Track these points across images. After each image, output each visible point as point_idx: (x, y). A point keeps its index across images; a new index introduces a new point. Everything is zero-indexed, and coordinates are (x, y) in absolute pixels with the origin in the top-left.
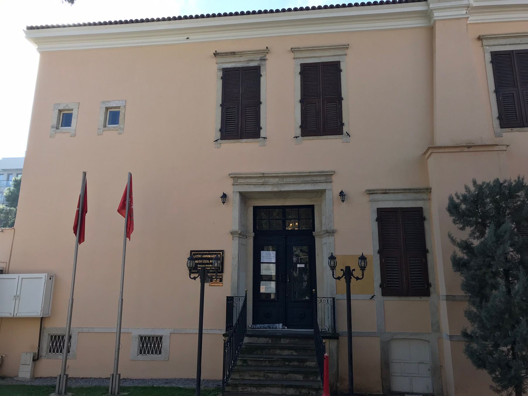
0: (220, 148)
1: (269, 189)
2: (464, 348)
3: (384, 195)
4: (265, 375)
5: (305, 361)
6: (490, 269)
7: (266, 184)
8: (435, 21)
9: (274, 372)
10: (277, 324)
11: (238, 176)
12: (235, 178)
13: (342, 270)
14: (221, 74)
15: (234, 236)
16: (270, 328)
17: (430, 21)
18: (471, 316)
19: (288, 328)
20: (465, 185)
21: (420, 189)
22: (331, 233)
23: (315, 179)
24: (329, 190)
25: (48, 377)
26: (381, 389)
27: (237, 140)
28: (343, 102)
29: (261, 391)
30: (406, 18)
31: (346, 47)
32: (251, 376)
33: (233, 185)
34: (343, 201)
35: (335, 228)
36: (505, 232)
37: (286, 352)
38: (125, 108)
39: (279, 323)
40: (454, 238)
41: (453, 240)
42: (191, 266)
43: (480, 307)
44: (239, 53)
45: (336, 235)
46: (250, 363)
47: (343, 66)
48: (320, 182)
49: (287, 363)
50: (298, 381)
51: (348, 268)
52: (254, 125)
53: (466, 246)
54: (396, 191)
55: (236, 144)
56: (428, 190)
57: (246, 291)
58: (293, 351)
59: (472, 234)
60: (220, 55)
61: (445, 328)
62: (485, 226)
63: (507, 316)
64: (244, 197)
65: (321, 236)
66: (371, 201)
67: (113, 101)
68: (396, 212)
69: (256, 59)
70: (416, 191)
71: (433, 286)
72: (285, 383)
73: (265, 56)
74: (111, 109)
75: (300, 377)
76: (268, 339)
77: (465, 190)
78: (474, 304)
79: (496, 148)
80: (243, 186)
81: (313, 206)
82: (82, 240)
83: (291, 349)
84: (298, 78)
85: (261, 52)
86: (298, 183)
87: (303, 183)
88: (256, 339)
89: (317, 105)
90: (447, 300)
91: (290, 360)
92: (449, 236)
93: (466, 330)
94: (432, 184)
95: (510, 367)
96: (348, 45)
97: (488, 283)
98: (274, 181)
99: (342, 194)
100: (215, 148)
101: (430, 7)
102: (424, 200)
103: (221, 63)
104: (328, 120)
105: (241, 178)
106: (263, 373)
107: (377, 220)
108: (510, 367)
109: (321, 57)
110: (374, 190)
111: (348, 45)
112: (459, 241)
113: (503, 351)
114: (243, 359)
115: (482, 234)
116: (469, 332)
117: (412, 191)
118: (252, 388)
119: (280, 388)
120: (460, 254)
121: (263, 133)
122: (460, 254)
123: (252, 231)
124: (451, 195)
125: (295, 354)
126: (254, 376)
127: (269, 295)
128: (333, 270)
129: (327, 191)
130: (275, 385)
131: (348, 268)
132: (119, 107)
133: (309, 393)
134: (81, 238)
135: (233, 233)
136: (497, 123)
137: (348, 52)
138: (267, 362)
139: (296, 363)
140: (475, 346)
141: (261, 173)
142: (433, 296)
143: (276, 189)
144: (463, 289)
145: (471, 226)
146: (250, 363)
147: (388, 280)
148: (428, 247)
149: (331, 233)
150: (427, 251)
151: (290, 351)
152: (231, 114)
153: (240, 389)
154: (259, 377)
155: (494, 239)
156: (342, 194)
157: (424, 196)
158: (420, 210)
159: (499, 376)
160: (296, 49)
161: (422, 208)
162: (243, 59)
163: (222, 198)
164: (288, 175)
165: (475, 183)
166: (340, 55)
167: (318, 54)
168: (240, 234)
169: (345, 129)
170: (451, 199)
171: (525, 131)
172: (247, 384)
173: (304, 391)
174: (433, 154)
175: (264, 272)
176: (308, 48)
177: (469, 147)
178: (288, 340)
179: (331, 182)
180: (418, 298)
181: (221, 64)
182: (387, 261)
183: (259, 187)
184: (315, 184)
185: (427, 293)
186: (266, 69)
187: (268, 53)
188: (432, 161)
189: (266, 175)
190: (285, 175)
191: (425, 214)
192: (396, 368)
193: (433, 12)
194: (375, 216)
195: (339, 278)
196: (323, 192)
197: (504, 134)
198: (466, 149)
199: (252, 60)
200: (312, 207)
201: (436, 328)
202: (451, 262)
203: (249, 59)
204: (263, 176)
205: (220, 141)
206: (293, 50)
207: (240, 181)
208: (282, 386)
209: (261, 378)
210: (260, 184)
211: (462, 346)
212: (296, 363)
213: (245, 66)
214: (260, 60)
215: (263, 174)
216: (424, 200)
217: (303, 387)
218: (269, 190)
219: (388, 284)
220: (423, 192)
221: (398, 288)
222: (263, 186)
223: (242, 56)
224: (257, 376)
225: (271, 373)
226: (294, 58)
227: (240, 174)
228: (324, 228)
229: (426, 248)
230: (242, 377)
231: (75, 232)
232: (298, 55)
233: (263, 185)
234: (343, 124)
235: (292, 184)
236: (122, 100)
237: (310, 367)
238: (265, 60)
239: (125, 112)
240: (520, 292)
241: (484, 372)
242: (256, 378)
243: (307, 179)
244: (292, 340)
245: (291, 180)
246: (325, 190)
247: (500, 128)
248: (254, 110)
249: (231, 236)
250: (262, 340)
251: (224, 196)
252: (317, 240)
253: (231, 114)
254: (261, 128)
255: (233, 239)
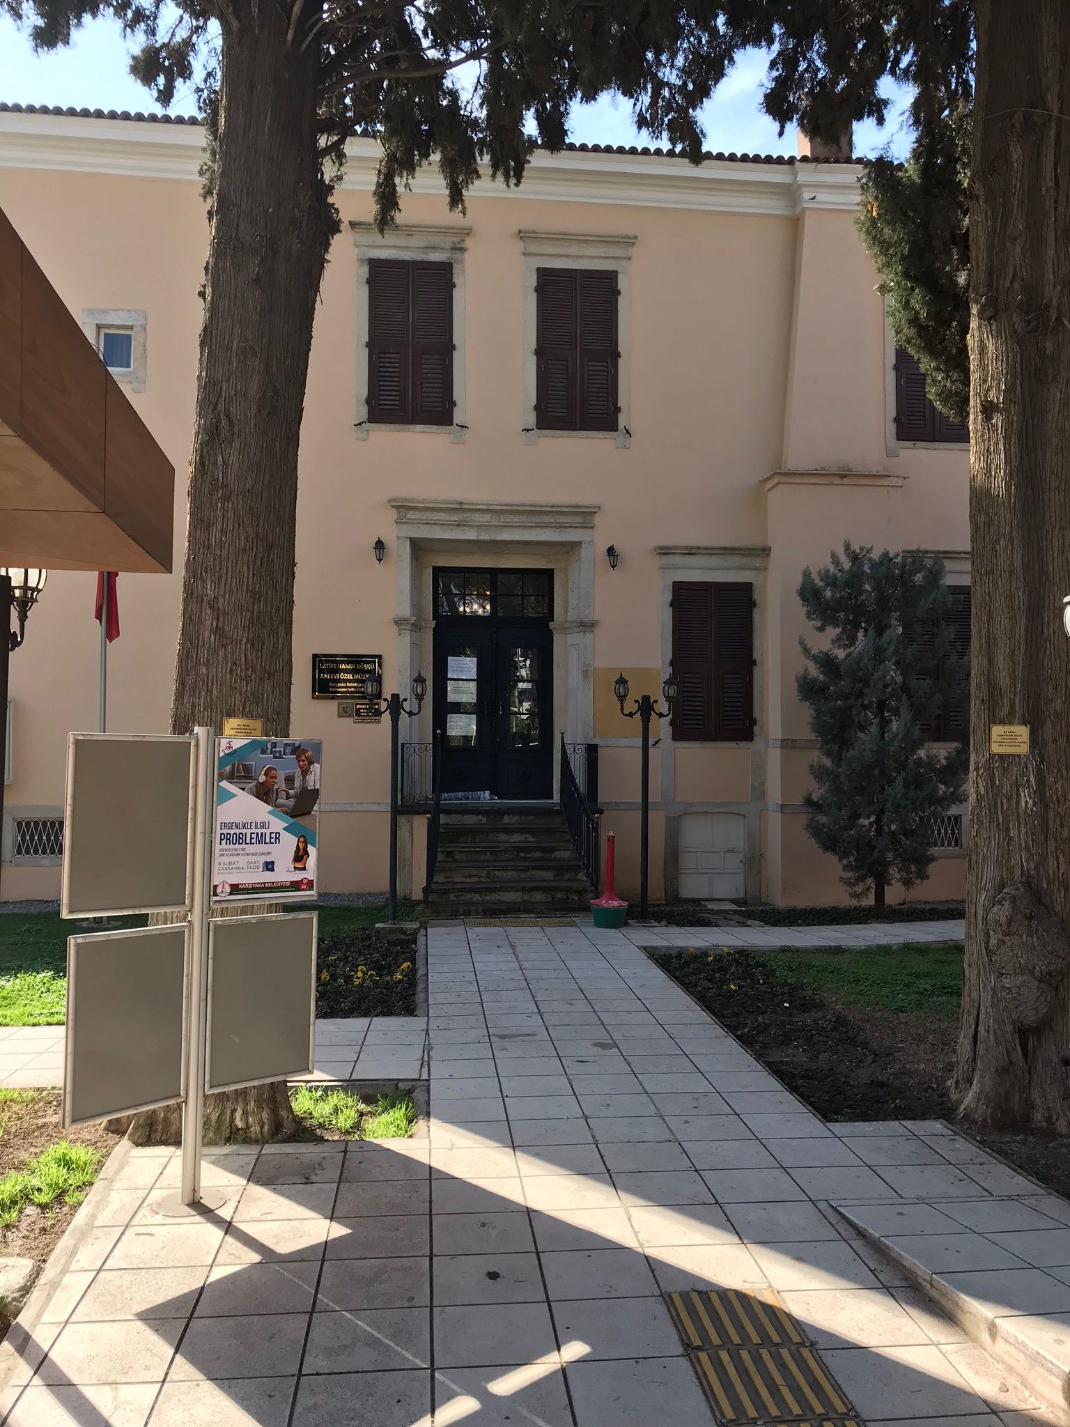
0: (366, 440)
1: (471, 535)
2: (805, 822)
3: (687, 557)
4: (489, 874)
5: (553, 850)
6: (860, 700)
7: (464, 525)
8: (804, 209)
9: (505, 869)
10: (480, 791)
11: (409, 504)
12: (403, 508)
13: (636, 701)
14: (365, 271)
15: (402, 627)
16: (467, 799)
17: (794, 206)
18: (819, 773)
19: (499, 799)
20: (832, 552)
21: (750, 549)
22: (588, 626)
23: (562, 519)
24: (589, 543)
25: (21, 902)
26: (663, 895)
27: (404, 426)
28: (621, 362)
29: (487, 898)
30: (751, 192)
31: (629, 241)
32: (465, 877)
33: (397, 523)
34: (614, 567)
35: (597, 616)
36: (889, 643)
37: (516, 838)
38: (145, 330)
39: (484, 791)
40: (808, 647)
41: (806, 650)
42: (374, 693)
43: (837, 759)
44: (408, 228)
45: (596, 630)
46: (457, 856)
47: (622, 284)
48: (571, 527)
49: (522, 855)
50: (545, 881)
51: (646, 698)
52: (440, 395)
53: (826, 662)
54: (710, 552)
55: (400, 433)
56: (765, 551)
57: (562, 734)
58: (528, 836)
59: (836, 641)
60: (363, 227)
61: (775, 794)
62: (857, 626)
63: (876, 772)
64: (419, 548)
65: (565, 631)
66: (664, 568)
67: (115, 310)
68: (707, 590)
69: (442, 245)
70: (743, 552)
71: (758, 723)
72: (528, 885)
73: (463, 241)
74: (109, 328)
75: (549, 875)
76: (480, 817)
77: (831, 560)
78: (828, 754)
79: (886, 482)
80: (418, 525)
81: (552, 571)
82: (114, 633)
83: (525, 833)
84: (532, 299)
85: (455, 231)
86: (529, 526)
87: (540, 527)
88: (459, 817)
89: (570, 364)
90: (782, 747)
91: (527, 850)
92: (801, 643)
93: (810, 794)
94: (775, 540)
95: (873, 848)
96: (636, 237)
97: (853, 721)
98: (482, 520)
99: (611, 551)
100: (357, 439)
101: (798, 179)
102: (756, 569)
103: (367, 246)
104: (590, 398)
105: (415, 509)
106: (485, 871)
107: (672, 604)
108: (873, 848)
109: (580, 257)
110: (669, 548)
111: (636, 237)
112: (815, 651)
113: (863, 826)
114: (447, 850)
115: (852, 640)
116: (815, 798)
117: (737, 552)
118: (473, 894)
119: (520, 893)
120: (814, 671)
121: (458, 416)
122: (814, 671)
123: (431, 617)
124: (808, 567)
125: (533, 839)
126: (470, 876)
127: (467, 739)
128: (622, 701)
129: (583, 545)
130: (511, 887)
131: (646, 698)
132: (131, 328)
133: (568, 898)
134: (112, 630)
135: (398, 622)
136: (892, 428)
137: (635, 251)
138: (488, 854)
139: (537, 854)
140: (823, 819)
141: (456, 501)
142: (758, 742)
143: (485, 537)
144: (814, 730)
145: (836, 626)
146: (457, 856)
147: (685, 712)
148: (757, 655)
149: (588, 626)
150: (754, 663)
151: (524, 836)
152: (389, 367)
153: (452, 897)
154: (480, 877)
155: (872, 653)
156: (611, 551)
157: (757, 562)
158: (747, 588)
159: (854, 863)
160: (529, 233)
161: (751, 583)
162: (415, 242)
163: (378, 551)
164: (510, 508)
165: (847, 547)
166: (618, 258)
167: (574, 250)
168: (412, 624)
169: (622, 421)
170: (806, 575)
171: (935, 449)
172: (464, 888)
173: (559, 895)
174: (781, 486)
175: (452, 697)
176: (555, 234)
177: (843, 477)
178: (516, 818)
179: (593, 527)
180: (732, 744)
181: (364, 248)
182: (686, 680)
183: (452, 530)
184: (562, 530)
185: (747, 735)
186: (464, 271)
187: (468, 234)
188: (779, 499)
189: (466, 507)
190: (504, 508)
191: (756, 596)
192: (687, 862)
193: (803, 189)
194: (669, 597)
195: (631, 715)
196: (575, 545)
197: (903, 453)
198: (838, 481)
199: (434, 248)
200: (550, 572)
201: (759, 792)
202: (796, 684)
203: (427, 244)
204: (460, 508)
205: (367, 426)
206: (522, 235)
207: (412, 515)
208: (523, 890)
209: (482, 879)
210: (453, 525)
211: (803, 820)
212: (537, 854)
213: (420, 259)
214: (452, 248)
215: (461, 504)
216: (756, 569)
217: (558, 889)
218: (472, 538)
219: (684, 719)
220: (755, 555)
221: (701, 727)
222: (459, 528)
223: (412, 235)
224: (476, 876)
225: (499, 870)
226: (524, 254)
227: (413, 501)
228: (572, 616)
229: (752, 656)
230: (449, 880)
231: (99, 616)
232: (533, 248)
233: (458, 525)
234: (618, 410)
235: (517, 527)
236: (135, 311)
237: (562, 859)
238: (462, 250)
239: (145, 341)
240: (900, 736)
241: (832, 859)
242: (474, 880)
243: (547, 519)
244: (523, 818)
245: (516, 519)
246: (581, 542)
247: (895, 441)
248: (440, 362)
249: (395, 628)
250: (470, 820)
251: (380, 545)
252: (557, 639)
253: (389, 367)
254: (454, 404)
255: (399, 635)
